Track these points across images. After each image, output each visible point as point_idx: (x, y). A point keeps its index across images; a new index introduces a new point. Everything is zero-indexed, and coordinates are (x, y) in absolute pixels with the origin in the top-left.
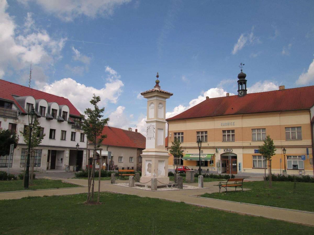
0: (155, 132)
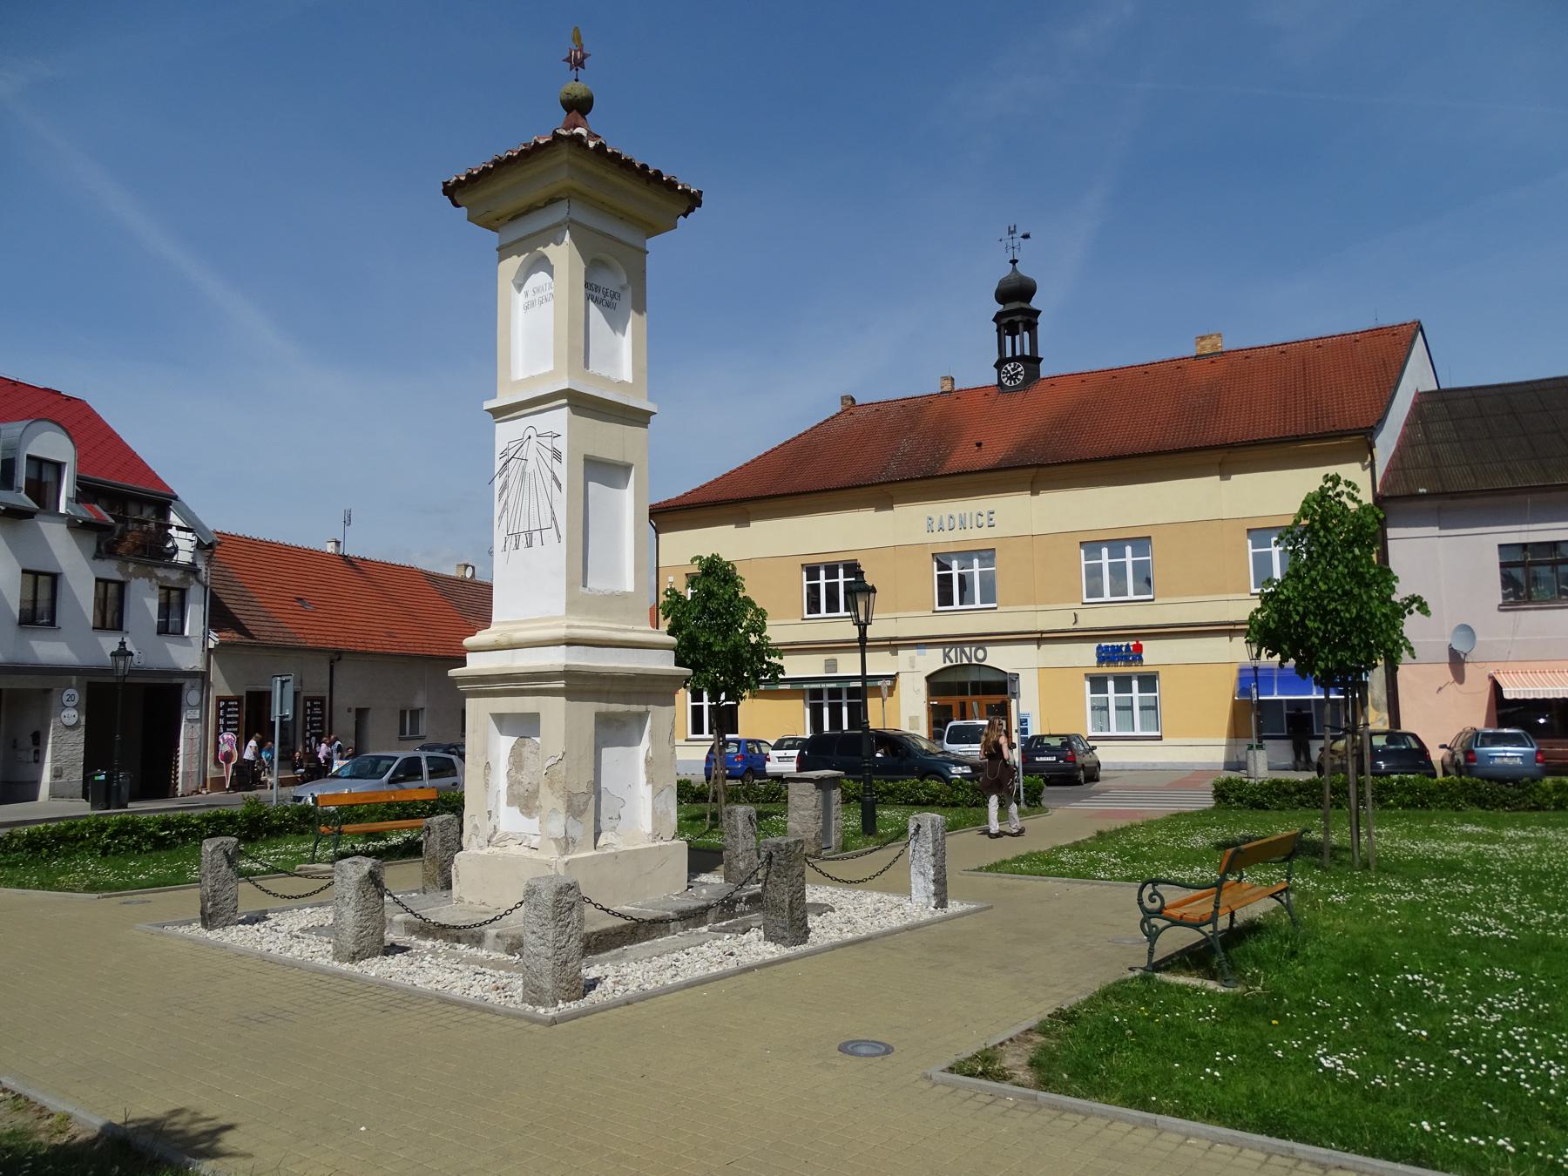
0: (563, 481)
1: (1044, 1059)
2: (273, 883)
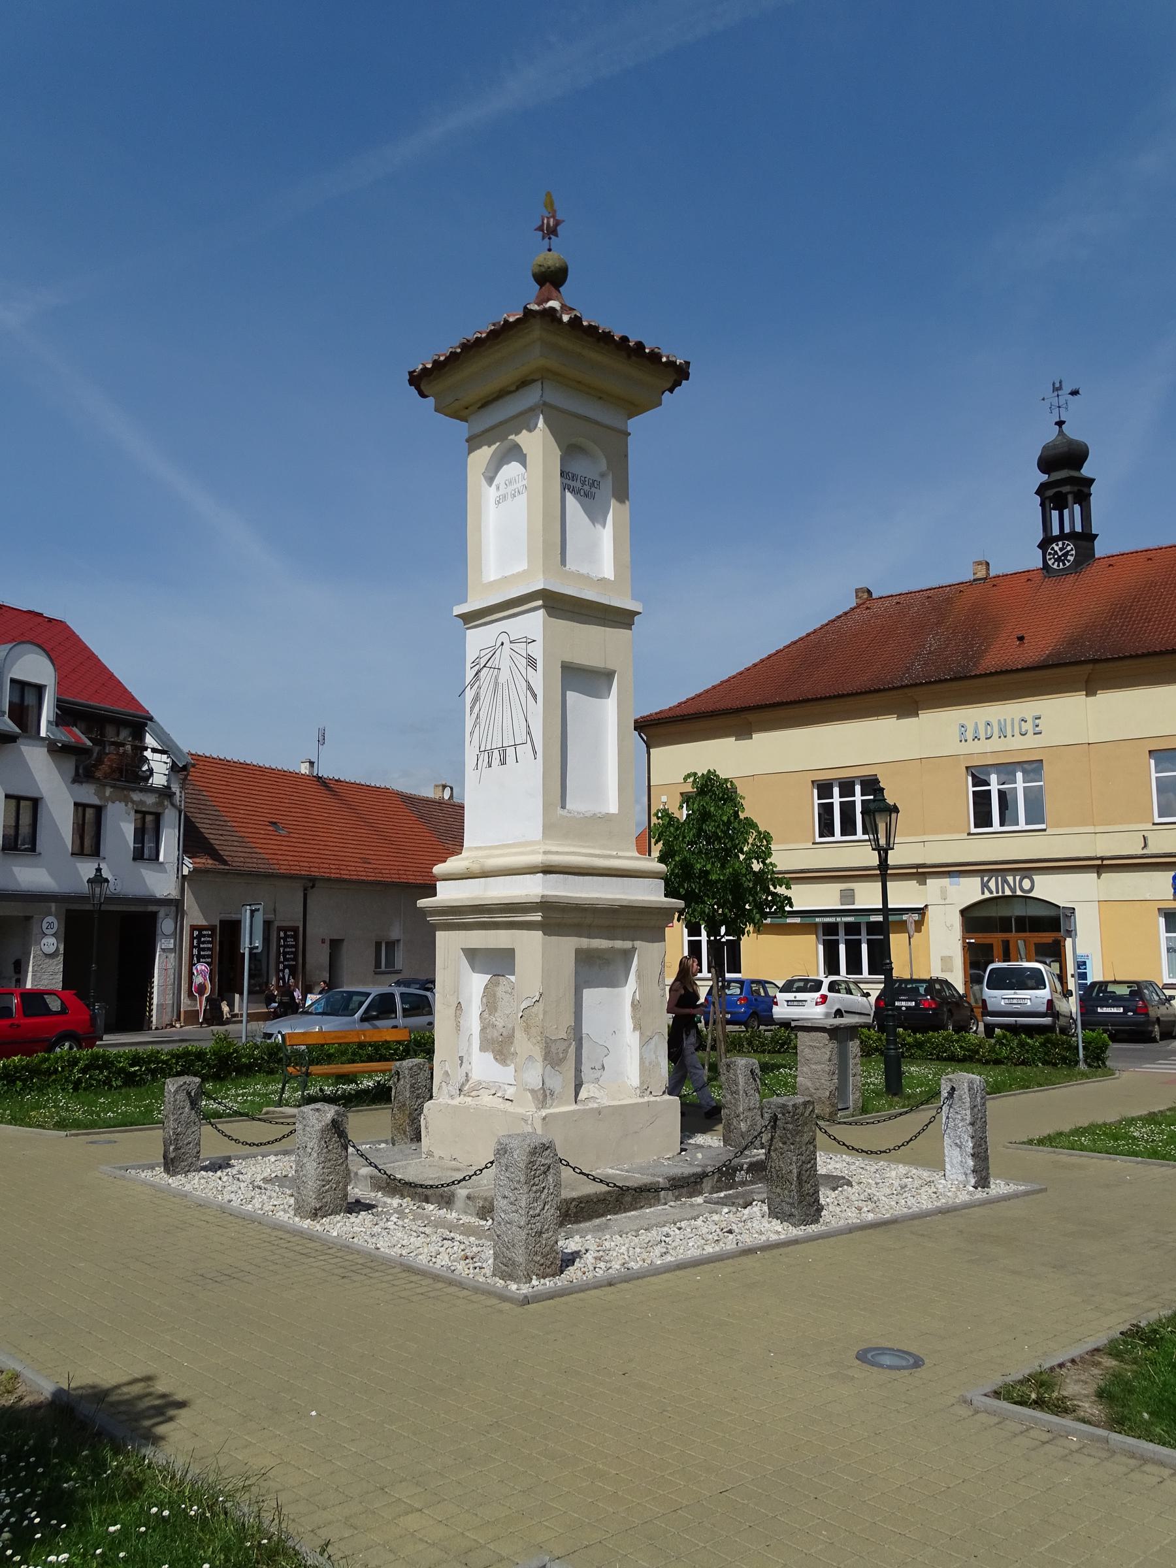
1: (1116, 1390)
2: (231, 1128)
